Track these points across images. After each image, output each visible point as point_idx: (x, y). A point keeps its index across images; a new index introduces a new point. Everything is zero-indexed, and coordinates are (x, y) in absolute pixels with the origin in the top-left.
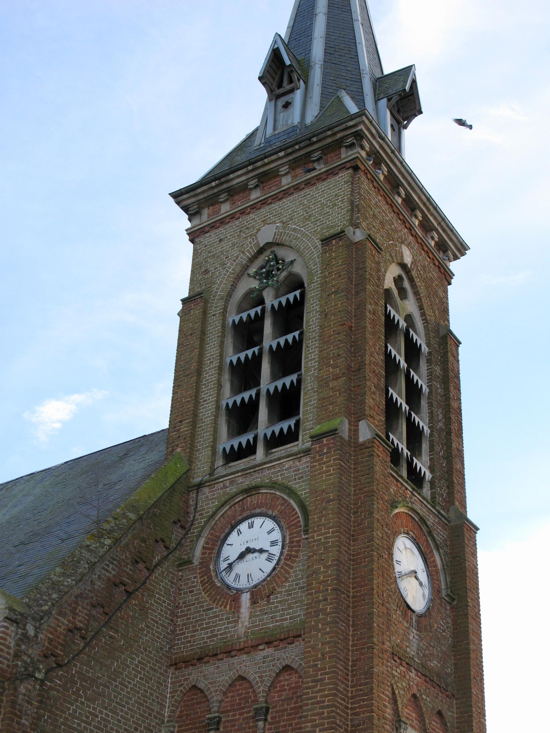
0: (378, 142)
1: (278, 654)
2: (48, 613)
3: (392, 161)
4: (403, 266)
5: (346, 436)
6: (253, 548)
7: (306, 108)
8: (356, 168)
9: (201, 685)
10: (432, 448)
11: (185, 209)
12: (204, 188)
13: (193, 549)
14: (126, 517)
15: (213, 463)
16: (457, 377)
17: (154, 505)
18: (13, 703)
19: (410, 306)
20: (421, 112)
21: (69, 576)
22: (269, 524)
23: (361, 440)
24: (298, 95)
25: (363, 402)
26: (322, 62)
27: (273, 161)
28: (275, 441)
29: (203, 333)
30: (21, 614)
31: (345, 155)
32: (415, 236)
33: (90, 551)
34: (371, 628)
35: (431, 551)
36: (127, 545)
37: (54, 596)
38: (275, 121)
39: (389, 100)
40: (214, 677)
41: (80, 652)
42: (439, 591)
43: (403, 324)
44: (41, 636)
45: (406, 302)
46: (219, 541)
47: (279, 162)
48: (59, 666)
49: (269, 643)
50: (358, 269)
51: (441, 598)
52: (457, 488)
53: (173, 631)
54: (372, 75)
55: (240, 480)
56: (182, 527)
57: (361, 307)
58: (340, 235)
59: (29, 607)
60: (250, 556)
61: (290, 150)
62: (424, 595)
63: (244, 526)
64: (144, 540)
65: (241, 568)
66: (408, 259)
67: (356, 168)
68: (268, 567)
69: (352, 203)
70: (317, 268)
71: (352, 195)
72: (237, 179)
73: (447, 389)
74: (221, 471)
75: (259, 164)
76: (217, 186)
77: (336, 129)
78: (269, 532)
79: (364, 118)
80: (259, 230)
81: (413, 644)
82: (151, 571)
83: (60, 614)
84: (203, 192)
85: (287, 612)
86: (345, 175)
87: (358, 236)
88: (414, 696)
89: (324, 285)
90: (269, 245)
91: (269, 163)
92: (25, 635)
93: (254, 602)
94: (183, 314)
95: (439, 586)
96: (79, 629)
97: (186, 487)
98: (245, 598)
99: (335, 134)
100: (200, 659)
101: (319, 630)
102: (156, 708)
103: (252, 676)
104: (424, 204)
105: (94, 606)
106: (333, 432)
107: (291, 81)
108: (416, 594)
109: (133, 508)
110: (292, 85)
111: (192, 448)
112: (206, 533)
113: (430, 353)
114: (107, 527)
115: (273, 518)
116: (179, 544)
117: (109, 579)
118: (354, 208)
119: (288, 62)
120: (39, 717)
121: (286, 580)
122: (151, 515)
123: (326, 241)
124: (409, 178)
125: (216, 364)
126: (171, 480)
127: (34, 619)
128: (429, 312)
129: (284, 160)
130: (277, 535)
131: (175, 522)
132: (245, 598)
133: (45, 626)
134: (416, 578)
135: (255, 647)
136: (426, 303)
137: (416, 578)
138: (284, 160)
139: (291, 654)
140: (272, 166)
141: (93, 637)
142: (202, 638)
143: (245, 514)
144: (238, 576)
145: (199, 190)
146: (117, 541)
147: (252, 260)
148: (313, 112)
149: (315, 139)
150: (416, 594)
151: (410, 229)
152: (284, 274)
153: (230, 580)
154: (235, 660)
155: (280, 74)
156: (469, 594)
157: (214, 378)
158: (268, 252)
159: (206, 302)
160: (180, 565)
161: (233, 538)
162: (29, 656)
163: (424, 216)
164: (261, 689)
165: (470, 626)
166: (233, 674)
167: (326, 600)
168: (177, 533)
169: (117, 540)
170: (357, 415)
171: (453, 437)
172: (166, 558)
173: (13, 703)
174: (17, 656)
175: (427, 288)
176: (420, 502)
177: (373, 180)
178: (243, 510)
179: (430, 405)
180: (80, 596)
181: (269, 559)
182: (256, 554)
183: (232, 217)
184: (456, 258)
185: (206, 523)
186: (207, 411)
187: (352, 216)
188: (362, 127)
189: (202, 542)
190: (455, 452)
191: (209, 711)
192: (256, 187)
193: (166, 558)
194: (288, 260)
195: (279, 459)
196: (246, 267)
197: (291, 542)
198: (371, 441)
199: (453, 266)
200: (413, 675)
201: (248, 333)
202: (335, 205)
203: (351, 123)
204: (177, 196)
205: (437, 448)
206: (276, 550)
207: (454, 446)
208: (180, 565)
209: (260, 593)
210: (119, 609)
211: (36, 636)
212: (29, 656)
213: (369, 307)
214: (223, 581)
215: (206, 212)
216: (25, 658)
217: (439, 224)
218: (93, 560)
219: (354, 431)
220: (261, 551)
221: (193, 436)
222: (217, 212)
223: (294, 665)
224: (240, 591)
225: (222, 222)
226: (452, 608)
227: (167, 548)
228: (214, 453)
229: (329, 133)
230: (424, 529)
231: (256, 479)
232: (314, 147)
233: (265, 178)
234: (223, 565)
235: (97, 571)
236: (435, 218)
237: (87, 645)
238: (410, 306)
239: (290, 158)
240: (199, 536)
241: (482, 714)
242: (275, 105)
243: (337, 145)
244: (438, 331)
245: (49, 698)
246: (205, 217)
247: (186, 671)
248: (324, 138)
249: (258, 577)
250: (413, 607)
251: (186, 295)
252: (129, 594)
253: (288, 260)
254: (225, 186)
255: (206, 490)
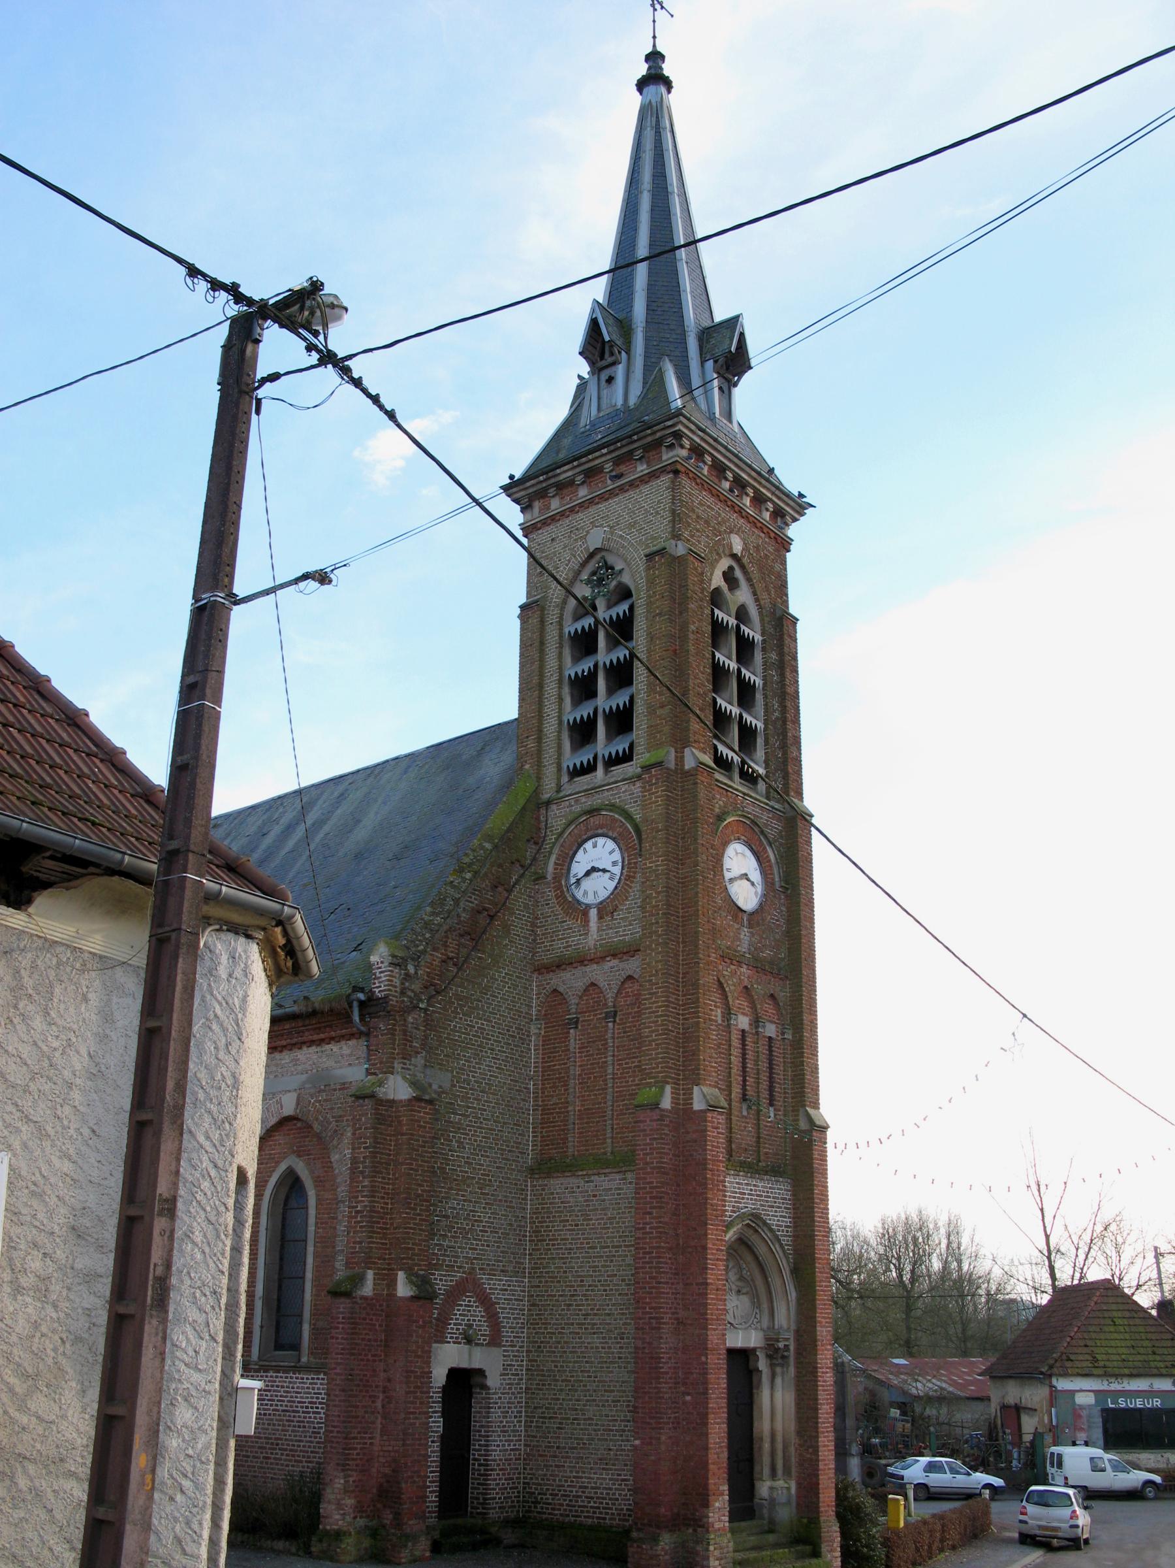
0: (699, 436)
1: (622, 965)
2: (424, 952)
3: (716, 449)
4: (734, 556)
5: (672, 766)
6: (598, 865)
7: (626, 389)
8: (676, 472)
9: (561, 989)
10: (766, 742)
11: (516, 501)
12: (533, 482)
13: (546, 864)
14: (482, 848)
15: (559, 779)
16: (795, 658)
17: (509, 830)
18: (405, 1032)
19: (743, 595)
20: (750, 368)
21: (437, 914)
22: (611, 844)
23: (686, 767)
24: (620, 370)
25: (687, 729)
26: (644, 324)
27: (597, 458)
28: (614, 761)
29: (542, 643)
30: (402, 958)
31: (667, 456)
32: (747, 517)
33: (454, 887)
34: (697, 946)
35: (765, 848)
36: (486, 874)
37: (428, 935)
38: (599, 398)
39: (716, 362)
40: (571, 982)
41: (455, 977)
42: (773, 884)
43: (733, 622)
44: (420, 972)
45: (738, 593)
46: (568, 858)
47: (603, 459)
48: (438, 993)
49: (614, 956)
50: (681, 586)
51: (774, 891)
52: (792, 777)
53: (534, 940)
54: (697, 323)
55: (583, 800)
56: (536, 843)
57: (684, 628)
58: (661, 552)
59: (408, 948)
60: (595, 875)
61: (612, 448)
62: (756, 893)
63: (588, 845)
64: (500, 866)
65: (586, 884)
66: (738, 548)
67: (676, 472)
68: (611, 885)
69: (673, 512)
70: (642, 582)
71: (673, 503)
72: (565, 474)
73: (782, 676)
74: (568, 789)
75: (584, 460)
76: (545, 480)
77: (655, 428)
78: (611, 853)
79: (681, 418)
80: (588, 532)
81: (745, 940)
82: (510, 891)
83: (435, 949)
84: (533, 485)
85: (626, 929)
86: (666, 479)
87: (680, 549)
88: (746, 987)
89: (649, 604)
90: (598, 550)
91: (593, 460)
92: (407, 975)
93: (600, 917)
94: (521, 617)
95: (773, 879)
96: (451, 959)
97: (537, 805)
98: (593, 913)
99: (654, 433)
100: (558, 966)
101: (652, 950)
102: (524, 1009)
103: (602, 984)
104: (755, 479)
105: (461, 936)
106: (659, 764)
107: (612, 354)
108: (747, 896)
109: (489, 838)
110: (613, 358)
111: (539, 764)
112: (556, 851)
113: (764, 641)
114: (466, 860)
115: (614, 839)
116: (534, 859)
117: (473, 908)
118: (676, 517)
119: (607, 338)
120: (426, 1037)
121: (627, 899)
122: (507, 840)
123: (650, 556)
124: (736, 460)
125: (556, 677)
126: (522, 802)
127: (413, 959)
128: (764, 596)
129: (609, 457)
130: (617, 856)
131: (528, 841)
132: (593, 913)
133: (423, 963)
134: (748, 880)
135: (603, 958)
136: (759, 587)
137: (748, 880)
138: (609, 457)
139: (632, 966)
140: (597, 462)
141: (465, 961)
142: (559, 948)
143: (589, 834)
144: (586, 893)
145: (528, 484)
146: (476, 873)
147: (583, 565)
148: (636, 389)
149: (635, 437)
150: (747, 896)
151: (740, 512)
152: (614, 583)
153: (579, 895)
154: (588, 969)
155: (597, 348)
156: (802, 883)
157: (555, 692)
158: (598, 557)
159: (543, 609)
160: (537, 879)
161: (580, 856)
162: (413, 991)
163: (756, 490)
164: (610, 996)
165: (802, 913)
166: (587, 981)
167: (657, 923)
168: (531, 850)
169: (476, 873)
170: (681, 741)
171: (790, 725)
172: (522, 876)
173: (405, 1032)
174: (403, 993)
175: (761, 569)
176: (754, 801)
177: (695, 478)
178: (587, 830)
179: (765, 696)
180: (450, 930)
181: (611, 879)
182: (600, 873)
183: (562, 514)
184: (795, 520)
185: (557, 839)
186: (550, 726)
187: (674, 527)
188: (680, 427)
189: (553, 858)
190: (790, 741)
191: (568, 1012)
192: (583, 483)
193: (522, 876)
194: (617, 568)
195: (616, 782)
196: (578, 573)
197: (629, 864)
198: (696, 769)
199: (793, 531)
200: (744, 969)
201: (585, 643)
202: (657, 513)
203: (669, 423)
204: (506, 489)
205: (772, 740)
206: (617, 870)
207: (790, 734)
208: (537, 879)
209: (606, 908)
210: (484, 933)
211: (416, 973)
212: (413, 991)
213: (692, 627)
214: (574, 896)
215: (537, 505)
216: (410, 993)
217: (773, 493)
218: (458, 896)
219: (680, 760)
220: (604, 871)
221: (539, 751)
222: (548, 508)
223: (636, 976)
224: (588, 906)
225: (553, 519)
226: (786, 896)
227: (522, 866)
228: (559, 769)
229: (649, 431)
230: (756, 829)
231: (596, 801)
232: (635, 446)
233: (591, 474)
234: (573, 880)
235: (462, 905)
236: (768, 489)
237: (460, 969)
238: (743, 595)
239: (614, 455)
240: (550, 853)
241: (813, 990)
242: (599, 379)
243: (657, 444)
244: (774, 613)
245: (433, 1020)
246: (536, 513)
247: (548, 976)
248: (645, 437)
249: (603, 895)
250: (744, 908)
251: (523, 600)
252: (492, 917)
253: (617, 568)
254: (552, 481)
255: (554, 807)
